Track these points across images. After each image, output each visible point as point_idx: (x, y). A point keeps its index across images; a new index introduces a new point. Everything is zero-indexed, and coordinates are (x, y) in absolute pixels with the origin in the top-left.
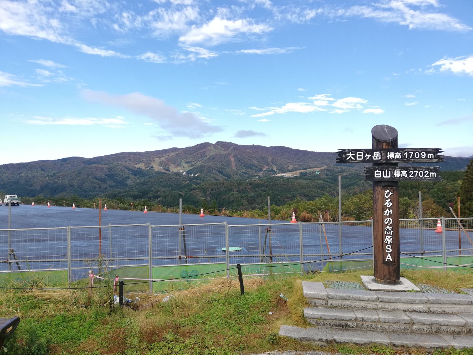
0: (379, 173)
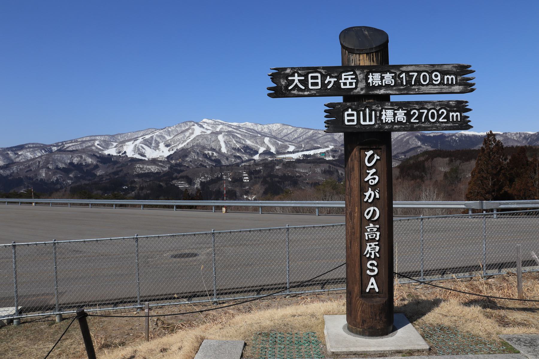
0: (352, 115)
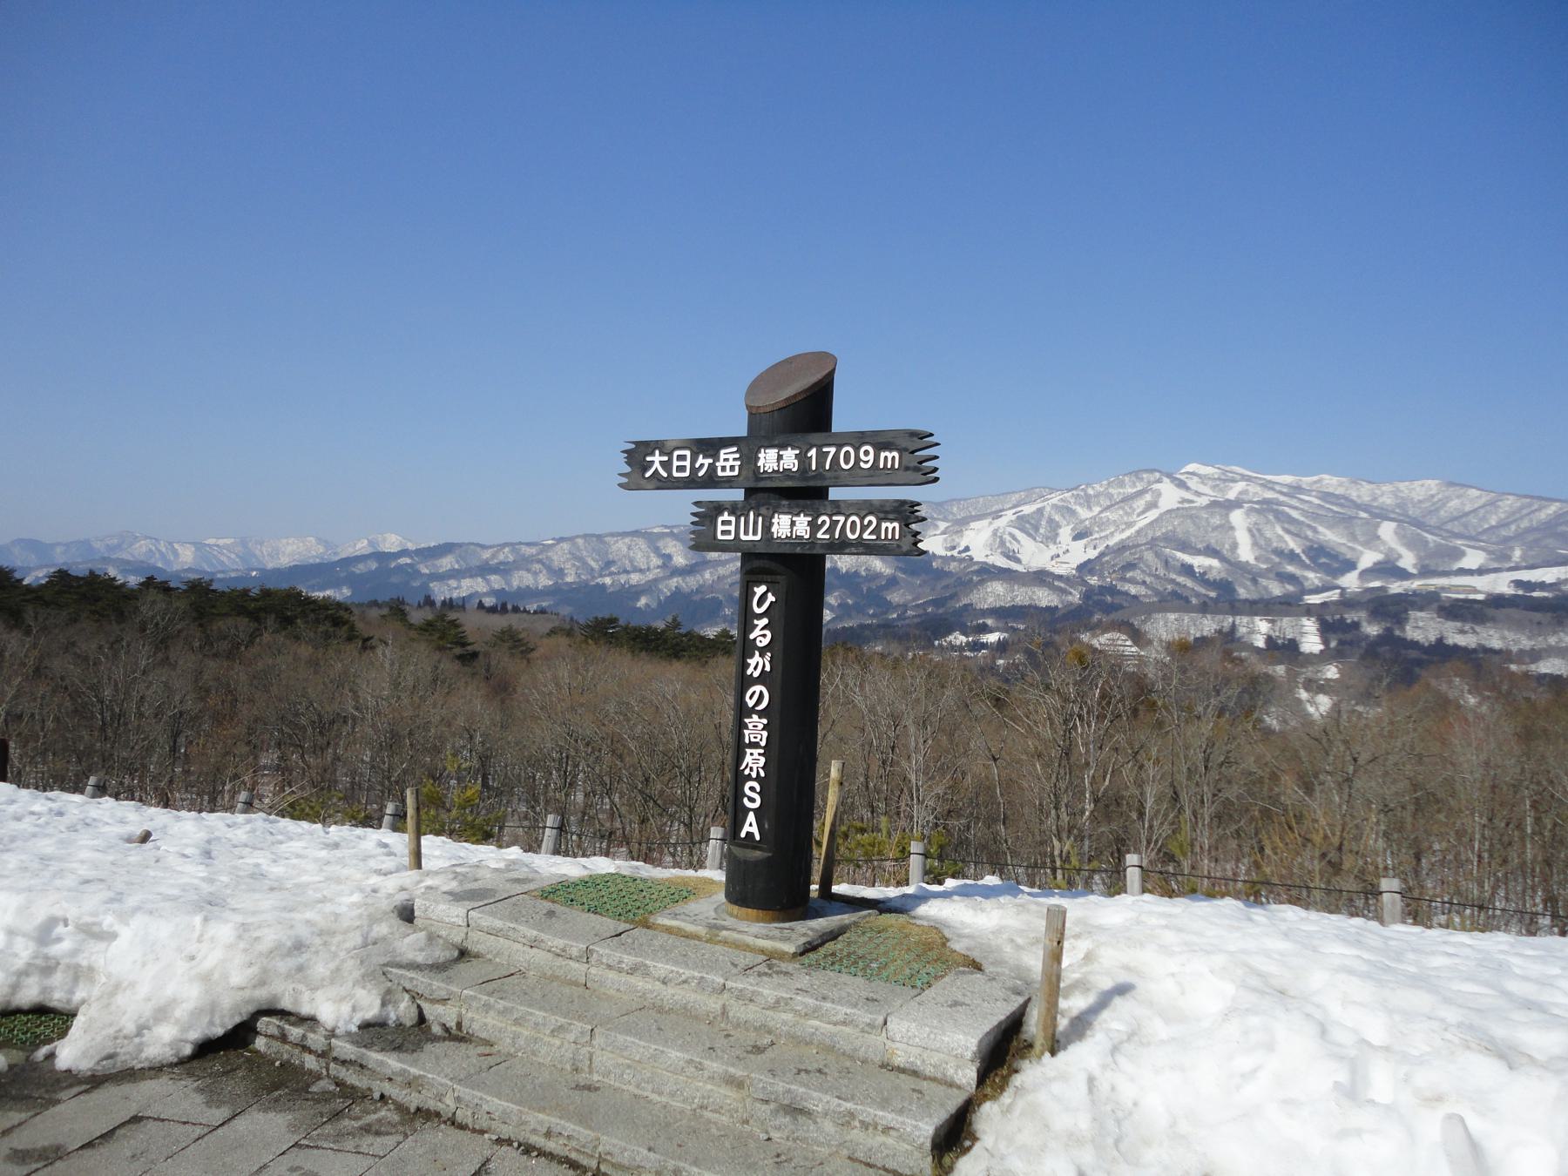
0: (729, 523)
